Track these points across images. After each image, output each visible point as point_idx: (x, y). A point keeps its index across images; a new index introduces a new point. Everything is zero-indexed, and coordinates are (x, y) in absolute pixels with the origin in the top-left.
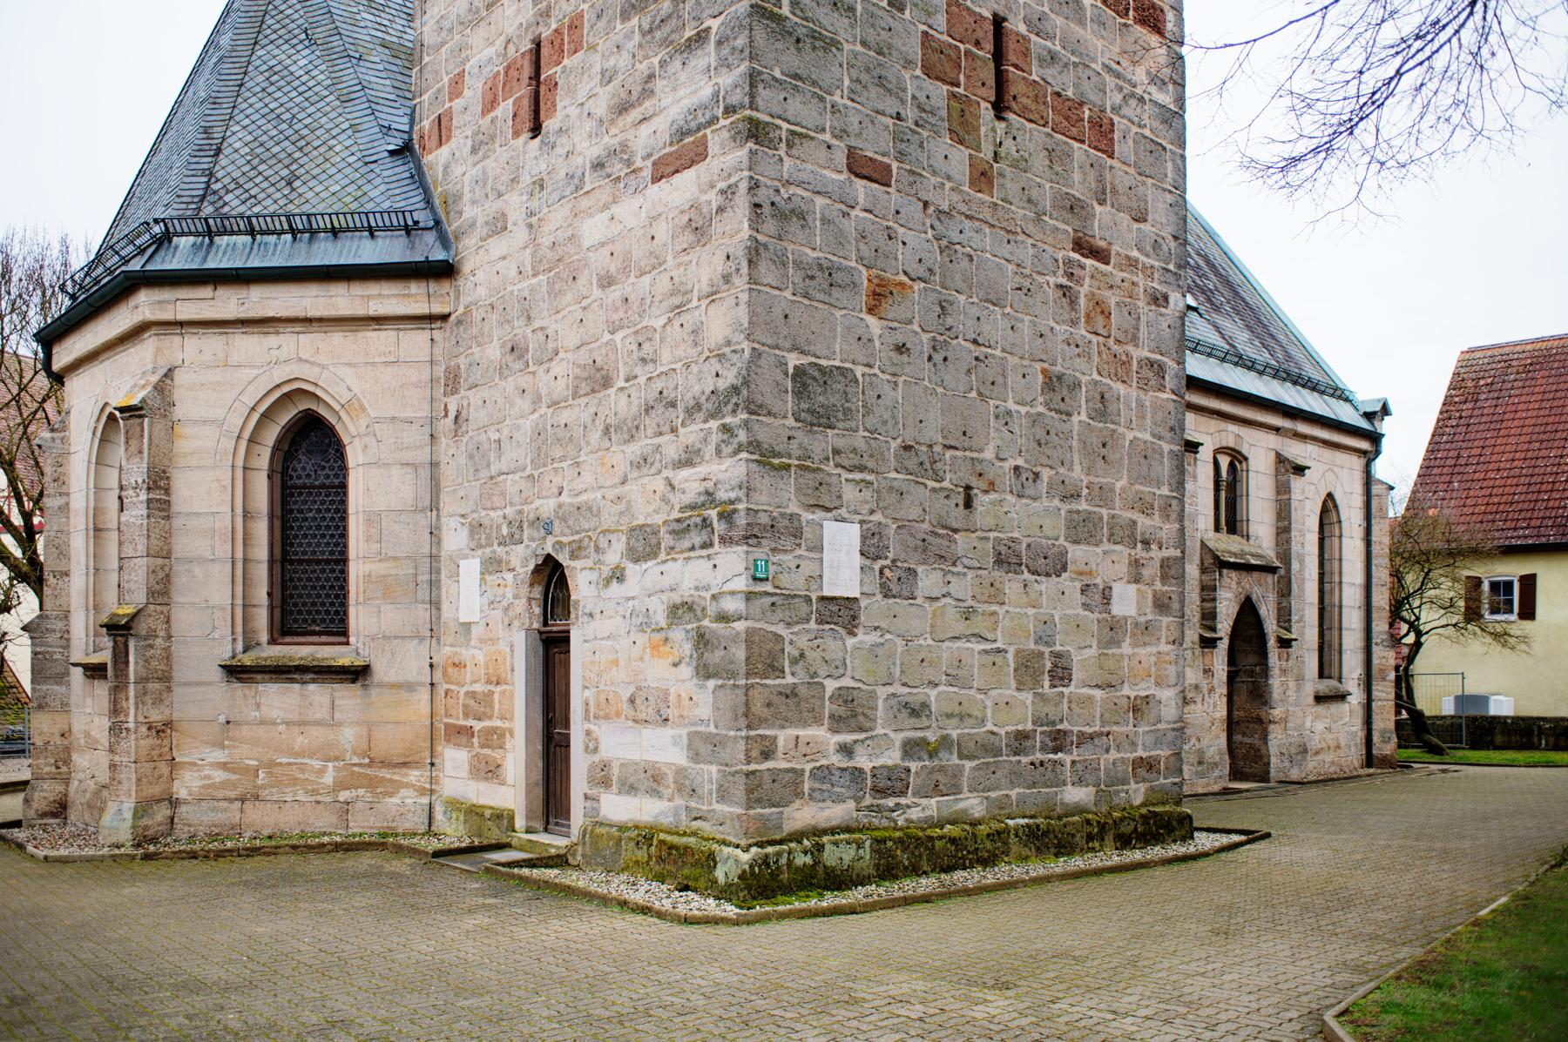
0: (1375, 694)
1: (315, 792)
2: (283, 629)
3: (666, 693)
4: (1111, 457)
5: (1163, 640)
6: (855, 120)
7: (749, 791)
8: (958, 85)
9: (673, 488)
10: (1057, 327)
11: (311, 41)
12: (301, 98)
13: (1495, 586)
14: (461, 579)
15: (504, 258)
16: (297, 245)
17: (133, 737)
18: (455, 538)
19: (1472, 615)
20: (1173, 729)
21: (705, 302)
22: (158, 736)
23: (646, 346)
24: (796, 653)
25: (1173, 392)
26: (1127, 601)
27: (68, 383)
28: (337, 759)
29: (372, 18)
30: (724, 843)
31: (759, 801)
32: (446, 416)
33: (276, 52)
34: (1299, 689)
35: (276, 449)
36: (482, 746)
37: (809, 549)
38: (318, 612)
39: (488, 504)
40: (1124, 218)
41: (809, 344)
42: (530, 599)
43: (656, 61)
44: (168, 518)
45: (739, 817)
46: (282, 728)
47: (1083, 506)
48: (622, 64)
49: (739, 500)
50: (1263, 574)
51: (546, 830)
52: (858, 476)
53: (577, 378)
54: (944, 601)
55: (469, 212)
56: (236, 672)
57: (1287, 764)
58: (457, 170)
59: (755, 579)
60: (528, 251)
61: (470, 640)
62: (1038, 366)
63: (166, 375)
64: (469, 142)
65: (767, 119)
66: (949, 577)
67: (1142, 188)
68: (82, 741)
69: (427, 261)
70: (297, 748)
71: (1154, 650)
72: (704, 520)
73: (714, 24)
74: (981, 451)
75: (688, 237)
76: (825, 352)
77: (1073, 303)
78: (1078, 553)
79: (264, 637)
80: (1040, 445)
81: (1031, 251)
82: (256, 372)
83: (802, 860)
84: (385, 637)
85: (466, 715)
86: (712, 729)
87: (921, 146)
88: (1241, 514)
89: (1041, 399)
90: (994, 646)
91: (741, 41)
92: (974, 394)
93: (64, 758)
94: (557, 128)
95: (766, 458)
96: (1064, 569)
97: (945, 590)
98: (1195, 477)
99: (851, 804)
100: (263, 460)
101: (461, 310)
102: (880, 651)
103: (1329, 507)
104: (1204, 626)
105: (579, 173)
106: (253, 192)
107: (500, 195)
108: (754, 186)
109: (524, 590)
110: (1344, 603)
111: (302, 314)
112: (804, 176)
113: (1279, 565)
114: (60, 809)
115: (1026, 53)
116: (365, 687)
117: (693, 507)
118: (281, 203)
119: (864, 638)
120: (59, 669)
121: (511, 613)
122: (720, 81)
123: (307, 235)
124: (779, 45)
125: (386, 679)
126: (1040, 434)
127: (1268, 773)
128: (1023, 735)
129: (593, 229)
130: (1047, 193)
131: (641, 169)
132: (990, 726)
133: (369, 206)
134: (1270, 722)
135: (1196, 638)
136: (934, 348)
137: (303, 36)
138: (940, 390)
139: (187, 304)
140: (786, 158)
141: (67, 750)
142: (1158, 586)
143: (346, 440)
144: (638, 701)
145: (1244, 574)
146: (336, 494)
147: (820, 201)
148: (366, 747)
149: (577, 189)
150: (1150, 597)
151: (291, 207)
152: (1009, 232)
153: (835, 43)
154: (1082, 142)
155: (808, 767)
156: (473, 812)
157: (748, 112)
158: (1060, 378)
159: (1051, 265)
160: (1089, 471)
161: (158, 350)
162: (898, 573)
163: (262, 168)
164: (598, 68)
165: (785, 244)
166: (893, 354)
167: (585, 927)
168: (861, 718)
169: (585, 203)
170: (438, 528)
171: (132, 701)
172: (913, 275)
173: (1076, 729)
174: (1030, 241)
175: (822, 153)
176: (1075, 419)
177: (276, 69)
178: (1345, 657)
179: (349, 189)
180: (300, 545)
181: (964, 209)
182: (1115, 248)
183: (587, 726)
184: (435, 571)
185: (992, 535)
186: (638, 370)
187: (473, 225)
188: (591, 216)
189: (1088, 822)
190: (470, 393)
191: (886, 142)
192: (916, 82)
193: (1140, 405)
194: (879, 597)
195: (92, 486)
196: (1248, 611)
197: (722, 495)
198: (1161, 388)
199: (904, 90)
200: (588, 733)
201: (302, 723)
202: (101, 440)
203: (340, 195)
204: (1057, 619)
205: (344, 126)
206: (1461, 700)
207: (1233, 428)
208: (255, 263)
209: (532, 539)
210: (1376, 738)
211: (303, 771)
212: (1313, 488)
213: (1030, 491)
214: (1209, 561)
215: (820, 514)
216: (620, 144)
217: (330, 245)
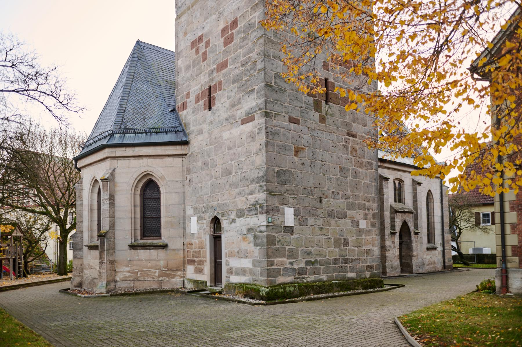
0: (446, 248)
1: (153, 278)
2: (144, 235)
3: (247, 250)
4: (358, 187)
6: (290, 109)
7: (268, 274)
8: (316, 97)
9: (248, 200)
11: (147, 81)
12: (145, 97)
13: (484, 215)
15: (202, 140)
16: (147, 136)
17: (106, 264)
18: (189, 211)
19: (478, 224)
21: (255, 155)
22: (112, 264)
23: (240, 165)
24: (278, 240)
25: (375, 170)
26: (363, 224)
27: (82, 171)
28: (159, 269)
29: (162, 73)
30: (262, 286)
31: (270, 276)
32: (187, 180)
33: (138, 84)
34: (421, 246)
35: (141, 189)
37: (281, 215)
38: (153, 231)
40: (361, 126)
41: (280, 165)
42: (210, 227)
43: (241, 95)
44: (114, 207)
45: (266, 280)
47: (351, 200)
48: (232, 95)
49: (264, 203)
50: (409, 214)
51: (215, 286)
52: (293, 196)
53: (222, 172)
54: (315, 226)
55: (192, 128)
56: (132, 247)
57: (418, 268)
58: (189, 117)
59: (268, 222)
60: (208, 139)
62: (338, 166)
63: (113, 171)
65: (269, 111)
66: (316, 220)
67: (365, 118)
68: (87, 266)
69: (182, 141)
70: (148, 267)
71: (371, 237)
72: (256, 208)
73: (256, 88)
74: (324, 188)
75: (250, 139)
76: (284, 166)
77: (347, 149)
79: (139, 238)
80: (339, 185)
81: (336, 137)
82: (137, 169)
83: (281, 290)
84: (171, 237)
85: (193, 257)
87: (307, 113)
88: (402, 197)
89: (339, 174)
90: (328, 237)
91: (263, 93)
92: (321, 174)
93: (81, 271)
95: (270, 193)
96: (346, 217)
97: (315, 223)
98: (388, 187)
99: (293, 277)
100: (138, 192)
101: (190, 153)
102: (299, 239)
103: (429, 194)
104: (391, 229)
105: (222, 120)
106: (134, 122)
107: (200, 125)
108: (267, 128)
109: (209, 225)
110: (435, 221)
112: (278, 124)
113: (414, 211)
114: (80, 285)
116: (166, 250)
117: (253, 205)
119: (295, 236)
120: (80, 247)
123: (149, 134)
124: (272, 93)
126: (339, 183)
127: (413, 271)
128: (336, 260)
129: (226, 135)
130: (339, 121)
132: (327, 257)
133: (165, 126)
134: (413, 256)
135: (389, 232)
136: (311, 163)
137: (145, 79)
138: (313, 174)
140: (274, 120)
141: (82, 269)
142: (372, 220)
143: (160, 186)
144: (240, 252)
145: (403, 214)
146: (157, 200)
147: (282, 130)
148: (166, 266)
149: (222, 125)
150: (370, 223)
152: (330, 132)
153: (286, 91)
155: (282, 268)
156: (195, 282)
157: (265, 110)
159: (341, 140)
160: (352, 191)
161: (111, 164)
162: (303, 219)
163: (136, 116)
164: (226, 95)
165: (274, 141)
166: (301, 166)
167: (230, 306)
168: (295, 256)
169: (223, 128)
170: (185, 209)
171: (105, 255)
172: (306, 146)
173: (350, 258)
174: (335, 134)
176: (348, 178)
177: (138, 89)
178: (436, 237)
179: (159, 121)
181: (318, 128)
182: (358, 134)
183: (226, 259)
184: (184, 220)
187: (193, 131)
188: (225, 132)
190: (193, 175)
191: (298, 114)
192: (305, 98)
193: (366, 174)
194: (299, 226)
195: (90, 198)
196: (405, 224)
197: (260, 202)
198: (372, 169)
199: (303, 100)
200: (227, 261)
201: (149, 260)
202: (93, 186)
203: (157, 123)
204: (345, 230)
205: (157, 104)
206: (475, 249)
207: (399, 173)
208: (136, 141)
209: (211, 212)
210: (446, 261)
211: (150, 272)
212: (424, 189)
213: (337, 197)
214: (393, 211)
215: (284, 206)
217: (155, 136)
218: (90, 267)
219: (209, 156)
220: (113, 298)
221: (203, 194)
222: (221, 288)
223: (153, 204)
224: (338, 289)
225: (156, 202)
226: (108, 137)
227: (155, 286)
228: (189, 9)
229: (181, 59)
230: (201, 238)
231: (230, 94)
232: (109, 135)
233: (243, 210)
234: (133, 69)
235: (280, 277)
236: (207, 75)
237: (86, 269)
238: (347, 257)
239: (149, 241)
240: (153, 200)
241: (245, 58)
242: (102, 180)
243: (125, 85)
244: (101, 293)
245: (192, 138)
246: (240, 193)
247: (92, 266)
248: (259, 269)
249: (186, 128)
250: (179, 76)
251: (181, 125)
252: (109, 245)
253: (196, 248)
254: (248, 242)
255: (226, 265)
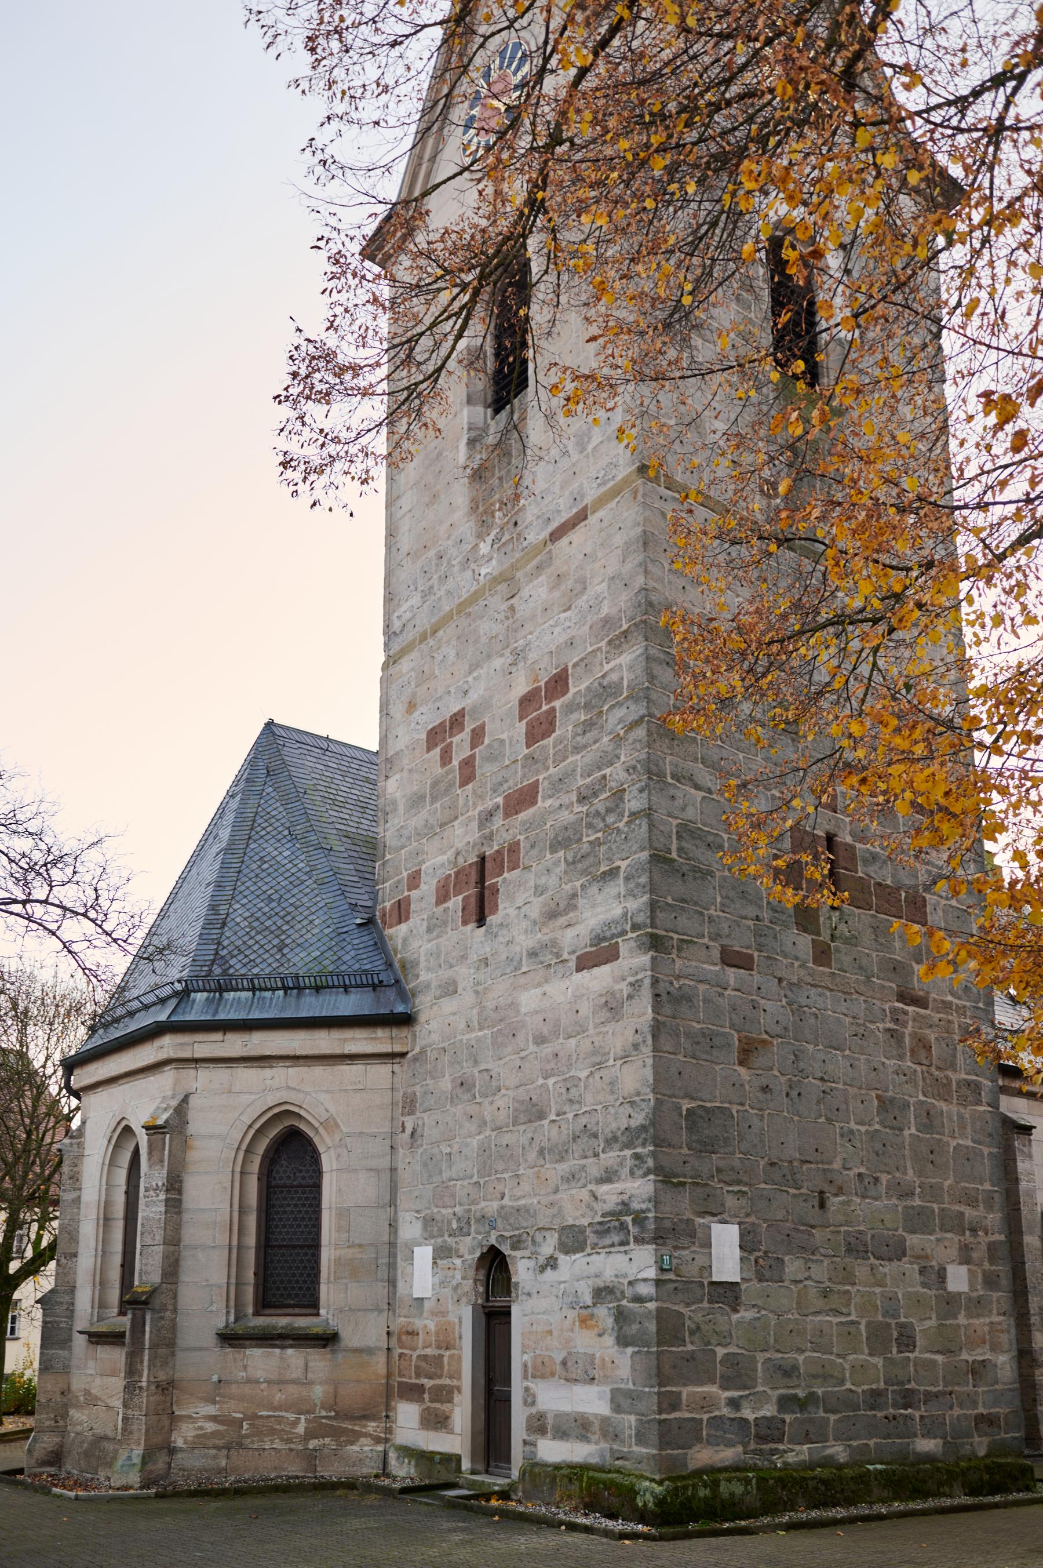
1: (289, 1441)
2: (265, 1303)
5: (995, 1311)
6: (725, 925)
7: (661, 1436)
9: (596, 1198)
10: (887, 1062)
11: (293, 837)
14: (415, 1262)
16: (288, 999)
18: (410, 1229)
20: (1010, 1390)
22: (163, 1394)
23: (573, 1091)
26: (958, 1279)
28: (308, 1412)
32: (403, 1131)
35: (264, 1157)
36: (431, 1401)
37: (701, 1246)
39: (440, 1203)
42: (475, 1281)
43: (578, 884)
44: (179, 1213)
45: (654, 1456)
46: (264, 1386)
47: (917, 1202)
51: (487, 1472)
52: (736, 1188)
53: (516, 1110)
54: (806, 1283)
55: (424, 976)
56: (229, 1338)
58: (415, 944)
60: (475, 1011)
61: (421, 1313)
62: (873, 1094)
64: (425, 924)
65: (664, 933)
66: (810, 1264)
69: (392, 1014)
70: (276, 1403)
71: (987, 1320)
72: (622, 1224)
74: (830, 1163)
75: (605, 1014)
78: (915, 1241)
81: (863, 1006)
82: (254, 1097)
83: (703, 1492)
84: (350, 1310)
85: (418, 1375)
86: (631, 1386)
87: (775, 937)
89: (877, 1119)
90: (849, 1319)
92: (823, 1120)
93: (62, 1414)
94: (499, 921)
96: (904, 1254)
97: (806, 1274)
99: (740, 1449)
100: (255, 1166)
101: (417, 1050)
102: (757, 1324)
105: (517, 958)
107: (451, 967)
108: (655, 982)
109: (472, 1273)
111: (292, 1053)
112: (690, 971)
114: (56, 1458)
115: (853, 858)
116: (333, 1352)
118: (275, 965)
119: (746, 1314)
121: (459, 1291)
122: (628, 905)
124: (670, 880)
125: (351, 1345)
126: (878, 1146)
128: (876, 1394)
129: (529, 1000)
131: (567, 960)
132: (848, 1385)
133: (344, 968)
136: (790, 1087)
137: (286, 832)
138: (796, 1118)
139: (202, 1045)
142: (987, 1265)
143: (321, 1149)
144: (569, 1364)
146: (311, 1192)
147: (702, 987)
149: (516, 969)
151: (282, 969)
154: (901, 917)
155: (705, 1417)
158: (892, 1100)
160: (920, 1173)
161: (177, 1081)
162: (770, 1262)
164: (532, 883)
166: (759, 1094)
169: (522, 980)
170: (396, 1221)
171: (146, 1363)
172: (772, 1033)
175: (704, 952)
176: (906, 1133)
180: (280, 1233)
181: (809, 980)
183: (526, 1384)
184: (392, 1255)
185: (842, 1229)
186: (567, 1108)
187: (428, 986)
189: (938, 1469)
190: (425, 1116)
191: (749, 938)
193: (961, 1117)
194: (755, 1282)
197: (636, 1206)
198: (979, 1103)
199: (761, 899)
202: (115, 1146)
204: (900, 1296)
208: (255, 1015)
209: (479, 1233)
211: (280, 1423)
215: (708, 1219)
216: (551, 940)
217: (313, 999)
218: (92, 1401)
219: (476, 1062)
220: (164, 1504)
221: (454, 1176)
222: (508, 1481)
223: (296, 1205)
224: (885, 1494)
225: (307, 1199)
226: (172, 1003)
227: (294, 1469)
228: (423, 638)
229: (397, 776)
230: (444, 1314)
231: (543, 880)
232: (176, 994)
233: (582, 1230)
234: (253, 802)
235: (697, 1447)
236: (475, 824)
237: (78, 1406)
238: (912, 1385)
239: (282, 1322)
240: (296, 1192)
241: (588, 780)
242: (147, 1128)
243: (229, 849)
244: (126, 1488)
245: (426, 1007)
246: (571, 1178)
247: (97, 1398)
248: (633, 1418)
249: (405, 976)
250: (388, 825)
251: (389, 965)
252: (156, 1330)
253: (430, 1346)
254: (596, 1331)
255: (525, 1403)
